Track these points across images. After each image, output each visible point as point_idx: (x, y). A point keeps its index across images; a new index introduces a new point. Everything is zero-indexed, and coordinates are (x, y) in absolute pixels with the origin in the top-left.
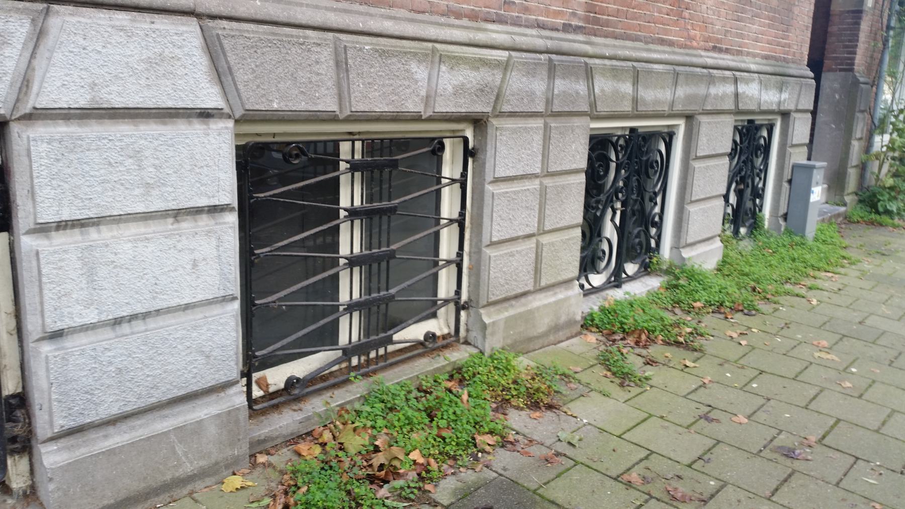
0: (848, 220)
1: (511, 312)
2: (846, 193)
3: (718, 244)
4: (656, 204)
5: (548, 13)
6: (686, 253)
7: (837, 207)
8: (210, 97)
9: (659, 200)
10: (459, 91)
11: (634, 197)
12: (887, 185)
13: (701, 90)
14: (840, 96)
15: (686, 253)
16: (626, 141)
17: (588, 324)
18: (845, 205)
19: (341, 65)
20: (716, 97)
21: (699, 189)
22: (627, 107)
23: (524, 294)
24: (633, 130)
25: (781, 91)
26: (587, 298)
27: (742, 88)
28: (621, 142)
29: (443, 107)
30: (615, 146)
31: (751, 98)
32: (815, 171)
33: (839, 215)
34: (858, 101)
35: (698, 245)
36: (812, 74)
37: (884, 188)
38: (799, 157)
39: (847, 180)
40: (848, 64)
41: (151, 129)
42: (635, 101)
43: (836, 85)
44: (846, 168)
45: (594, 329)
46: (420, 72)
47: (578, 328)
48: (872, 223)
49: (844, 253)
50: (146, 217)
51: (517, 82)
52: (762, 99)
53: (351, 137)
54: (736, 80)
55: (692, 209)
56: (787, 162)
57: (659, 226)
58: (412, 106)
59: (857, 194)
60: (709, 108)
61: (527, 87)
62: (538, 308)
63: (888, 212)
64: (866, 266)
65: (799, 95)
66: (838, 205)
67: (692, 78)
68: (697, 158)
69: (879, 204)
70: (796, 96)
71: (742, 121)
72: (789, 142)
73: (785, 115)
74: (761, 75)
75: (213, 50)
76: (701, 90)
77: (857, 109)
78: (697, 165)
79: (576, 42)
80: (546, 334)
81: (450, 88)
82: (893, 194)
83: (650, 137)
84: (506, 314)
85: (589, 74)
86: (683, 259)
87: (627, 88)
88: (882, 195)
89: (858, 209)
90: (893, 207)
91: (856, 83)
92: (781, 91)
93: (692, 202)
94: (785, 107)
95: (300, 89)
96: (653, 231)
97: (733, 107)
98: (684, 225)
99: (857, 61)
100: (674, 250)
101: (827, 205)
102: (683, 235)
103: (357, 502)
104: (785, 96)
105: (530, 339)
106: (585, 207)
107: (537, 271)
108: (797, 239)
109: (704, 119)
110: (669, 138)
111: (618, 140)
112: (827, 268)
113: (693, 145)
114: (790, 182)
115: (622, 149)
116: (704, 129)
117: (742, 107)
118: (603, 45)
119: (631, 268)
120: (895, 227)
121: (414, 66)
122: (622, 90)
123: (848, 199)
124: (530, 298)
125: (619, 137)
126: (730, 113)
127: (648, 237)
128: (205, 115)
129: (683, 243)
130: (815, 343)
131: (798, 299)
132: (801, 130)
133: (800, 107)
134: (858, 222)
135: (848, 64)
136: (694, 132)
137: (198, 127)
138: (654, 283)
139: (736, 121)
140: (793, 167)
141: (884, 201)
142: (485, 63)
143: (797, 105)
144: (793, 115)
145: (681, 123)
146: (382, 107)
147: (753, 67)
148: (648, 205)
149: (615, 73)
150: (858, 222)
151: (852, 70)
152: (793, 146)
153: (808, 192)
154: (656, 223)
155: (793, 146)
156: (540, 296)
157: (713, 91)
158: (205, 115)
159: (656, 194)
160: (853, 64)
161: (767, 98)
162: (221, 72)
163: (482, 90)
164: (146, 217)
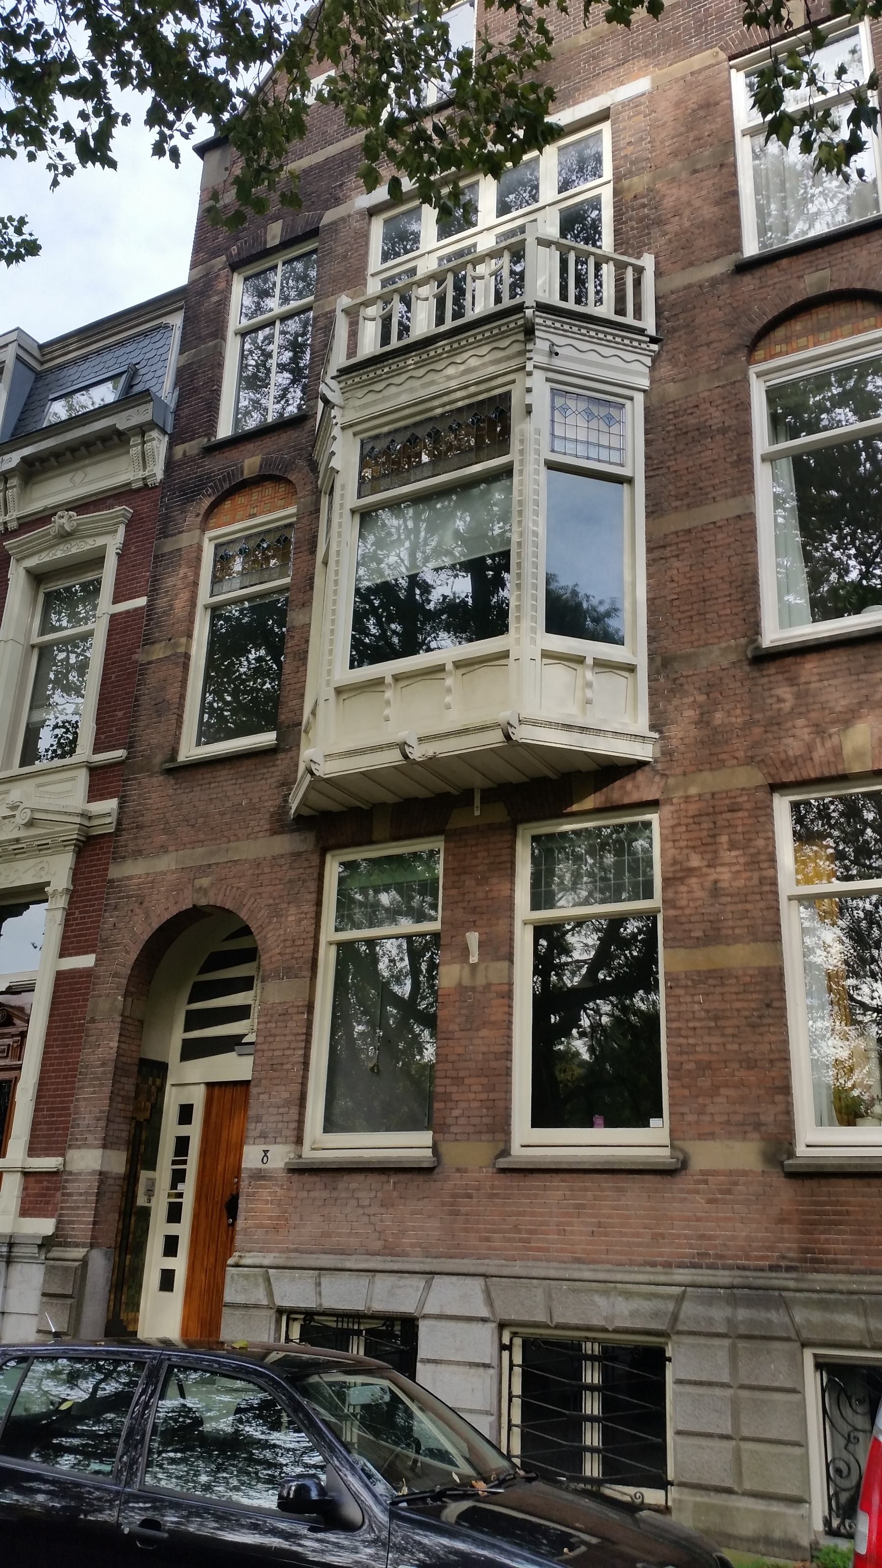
1: (706, 1499)
5: (748, 1258)
8: (484, 1312)
10: (633, 1314)
19: (549, 1297)
29: (620, 1323)
46: (601, 1301)
50: (458, 1363)
53: (594, 1340)
58: (596, 1321)
62: (738, 1509)
75: (487, 1292)
80: (747, 1540)
81: (626, 1313)
84: (699, 1499)
95: (531, 1307)
105: (730, 1537)
121: (597, 1298)
128: (484, 1320)
137: (480, 1324)
142: (639, 1294)
146: (574, 1321)
158: (484, 1320)
162: (490, 1301)
164: (458, 1363)
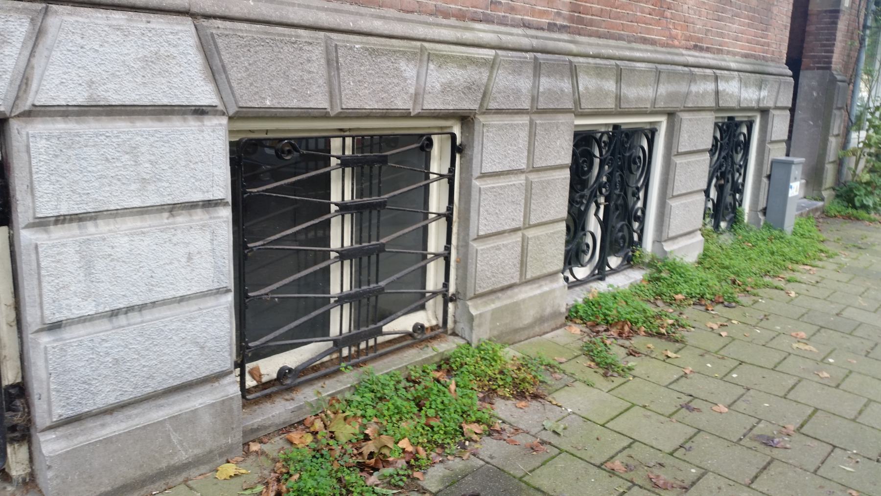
0: (825, 214)
1: (498, 304)
2: (823, 188)
3: (699, 238)
4: (638, 198)
5: (533, 13)
6: (668, 247)
7: (815, 202)
8: (204, 94)
9: (641, 194)
10: (447, 88)
11: (617, 192)
12: (864, 180)
13: (683, 88)
14: (818, 94)
15: (668, 247)
16: (609, 138)
17: (572, 316)
18: (823, 199)
19: (332, 63)
20: (697, 94)
21: (680, 184)
22: (610, 104)
23: (511, 287)
24: (616, 127)
25: (760, 89)
26: (571, 290)
27: (722, 86)
28: (605, 138)
29: (431, 104)
30: (599, 142)
31: (731, 96)
32: (793, 167)
33: (817, 210)
34: (835, 98)
35: (680, 239)
36: (790, 73)
37: (861, 183)
38: (778, 153)
39: (824, 176)
40: (825, 63)
41: (147, 126)
42: (618, 98)
43: (814, 83)
44: (824, 164)
45: (578, 321)
46: (409, 70)
47: (563, 319)
48: (849, 217)
49: (821, 246)
50: (143, 211)
51: (503, 80)
52: (742, 96)
53: (342, 134)
54: (716, 78)
55: (673, 203)
56: (766, 158)
57: (642, 220)
58: (401, 103)
59: (834, 189)
60: (690, 105)
61: (513, 84)
62: (524, 300)
63: (864, 207)
64: (843, 259)
65: (778, 93)
66: (816, 200)
67: (673, 76)
68: (679, 154)
69: (856, 199)
70: (775, 94)
71: (722, 117)
72: (768, 138)
73: (764, 112)
74: (741, 74)
75: (208, 49)
76: (683, 88)
77: (834, 106)
78: (678, 160)
79: (561, 41)
80: (531, 326)
81: (438, 86)
82: (869, 189)
83: (632, 133)
84: (493, 306)
85: (573, 72)
86: (665, 252)
87: (610, 85)
88: (859, 190)
89: (835, 203)
90: (869, 201)
91: (833, 80)
92: (760, 89)
93: (673, 197)
94: (764, 104)
96: (636, 225)
97: (714, 105)
98: (666, 219)
99: (834, 60)
100: (657, 244)
101: (805, 200)
102: (665, 229)
103: (348, 489)
104: (764, 93)
105: (516, 331)
106: (569, 202)
107: (523, 264)
108: (776, 233)
109: (685, 116)
110: (651, 134)
111: (601, 137)
112: (805, 261)
113: (675, 141)
114: (769, 177)
115: (605, 145)
116: (685, 126)
117: (722, 104)
118: (587, 44)
119: (614, 261)
120: (871, 221)
121: (403, 65)
122: (606, 87)
123: (825, 194)
124: (516, 290)
125: (603, 133)
126: (711, 110)
127: (631, 231)
128: (200, 112)
129: (664, 236)
130: (794, 334)
131: (777, 291)
132: (779, 126)
133: (779, 104)
134: (835, 216)
135: (825, 63)
136: (676, 128)
137: (192, 124)
138: (636, 276)
139: (716, 118)
140: (772, 162)
141: (860, 196)
142: (472, 61)
143: (776, 103)
144: (772, 112)
145: (663, 120)
146: (371, 104)
147: (733, 65)
148: (631, 200)
149: (599, 72)
150: (835, 216)
151: (829, 68)
152: (772, 142)
153: (786, 187)
154: (639, 217)
155: (772, 142)
156: (526, 288)
157: (694, 88)
158: (200, 112)
159: (638, 189)
160: (830, 63)
161: (746, 95)
162: (215, 70)
163: (469, 88)
164: (143, 211)
